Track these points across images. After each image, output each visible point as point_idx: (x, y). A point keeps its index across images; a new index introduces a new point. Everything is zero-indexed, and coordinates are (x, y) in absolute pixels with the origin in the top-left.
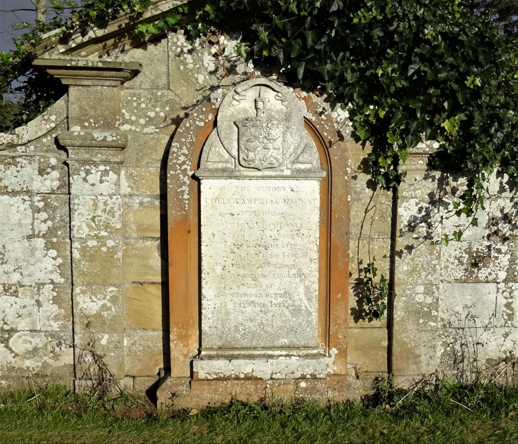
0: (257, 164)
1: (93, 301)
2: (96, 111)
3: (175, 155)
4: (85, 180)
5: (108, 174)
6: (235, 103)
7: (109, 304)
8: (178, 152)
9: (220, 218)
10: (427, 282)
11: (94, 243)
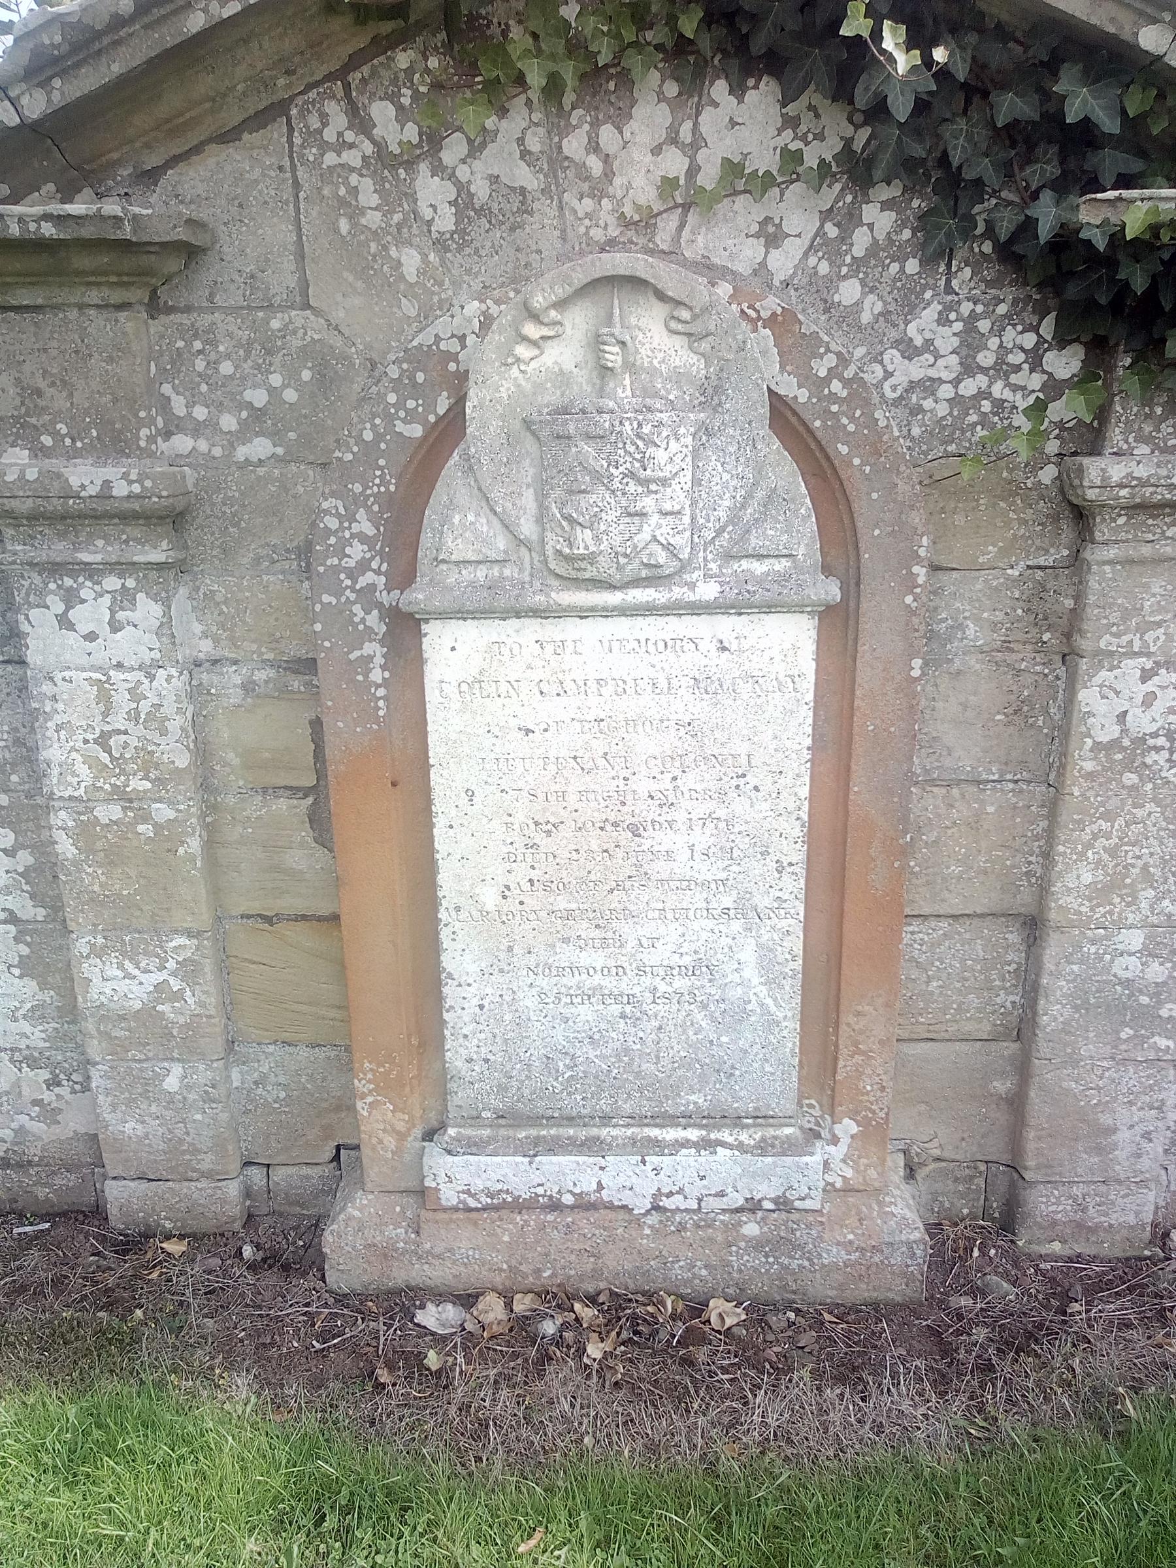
0: (606, 567)
1: (128, 976)
2: (71, 395)
3: (332, 540)
4: (64, 622)
5: (133, 602)
6: (522, 351)
7: (175, 984)
8: (341, 529)
9: (488, 741)
10: (1154, 919)
11: (115, 812)
